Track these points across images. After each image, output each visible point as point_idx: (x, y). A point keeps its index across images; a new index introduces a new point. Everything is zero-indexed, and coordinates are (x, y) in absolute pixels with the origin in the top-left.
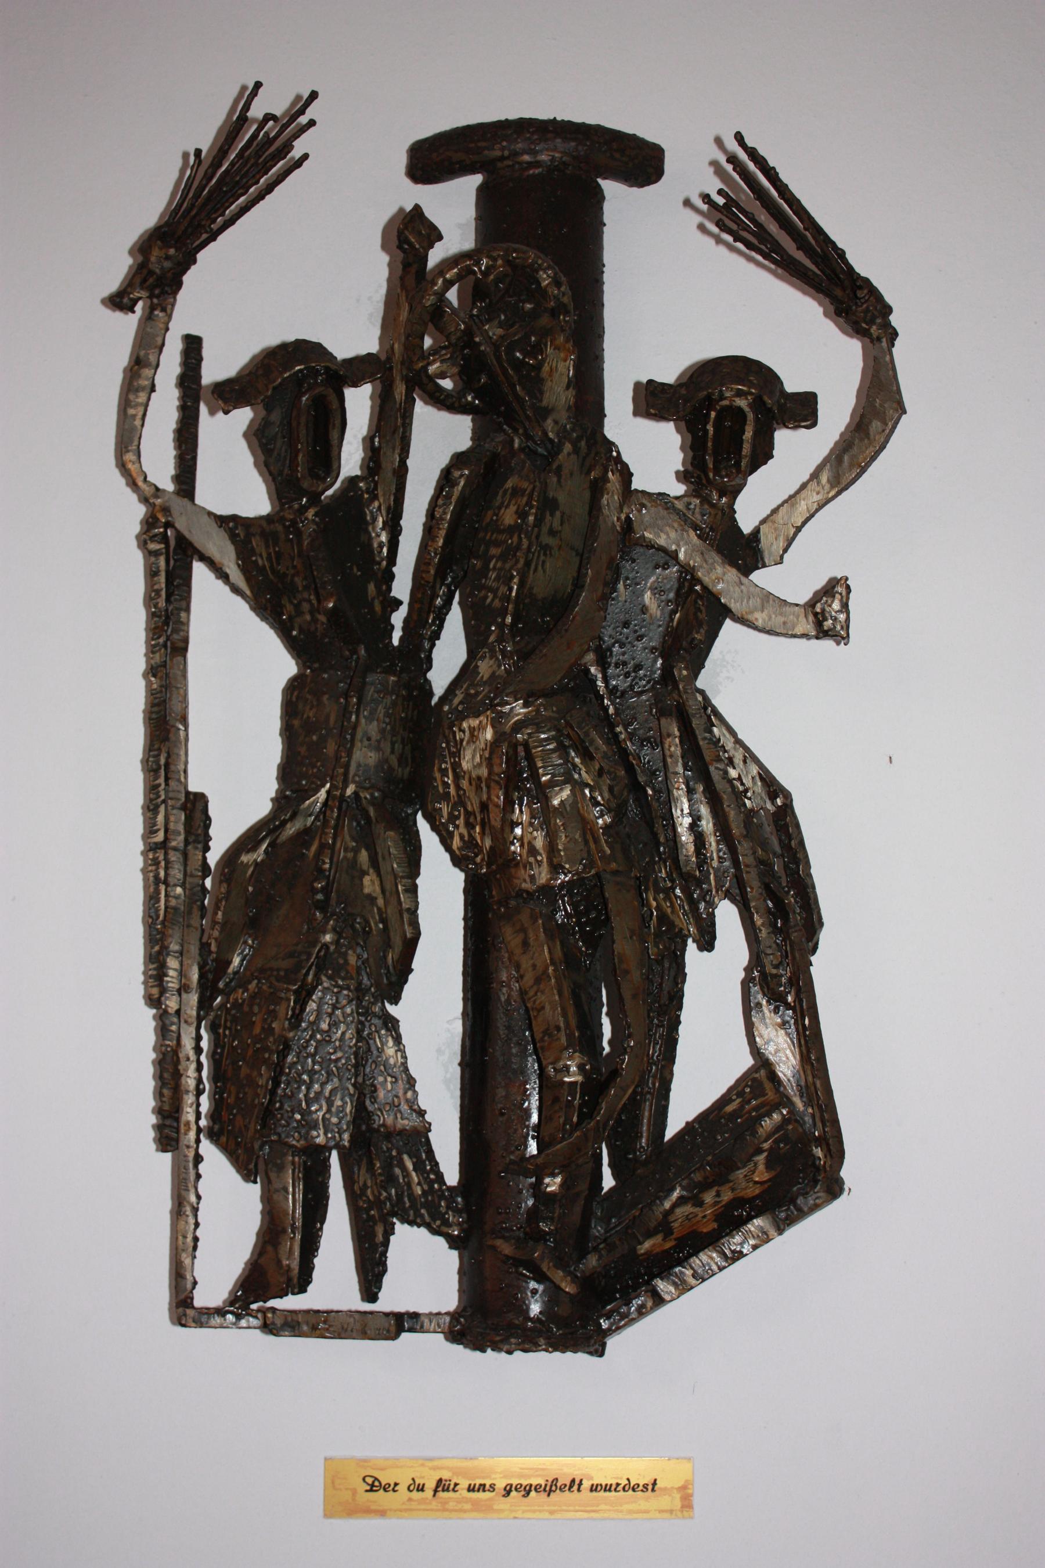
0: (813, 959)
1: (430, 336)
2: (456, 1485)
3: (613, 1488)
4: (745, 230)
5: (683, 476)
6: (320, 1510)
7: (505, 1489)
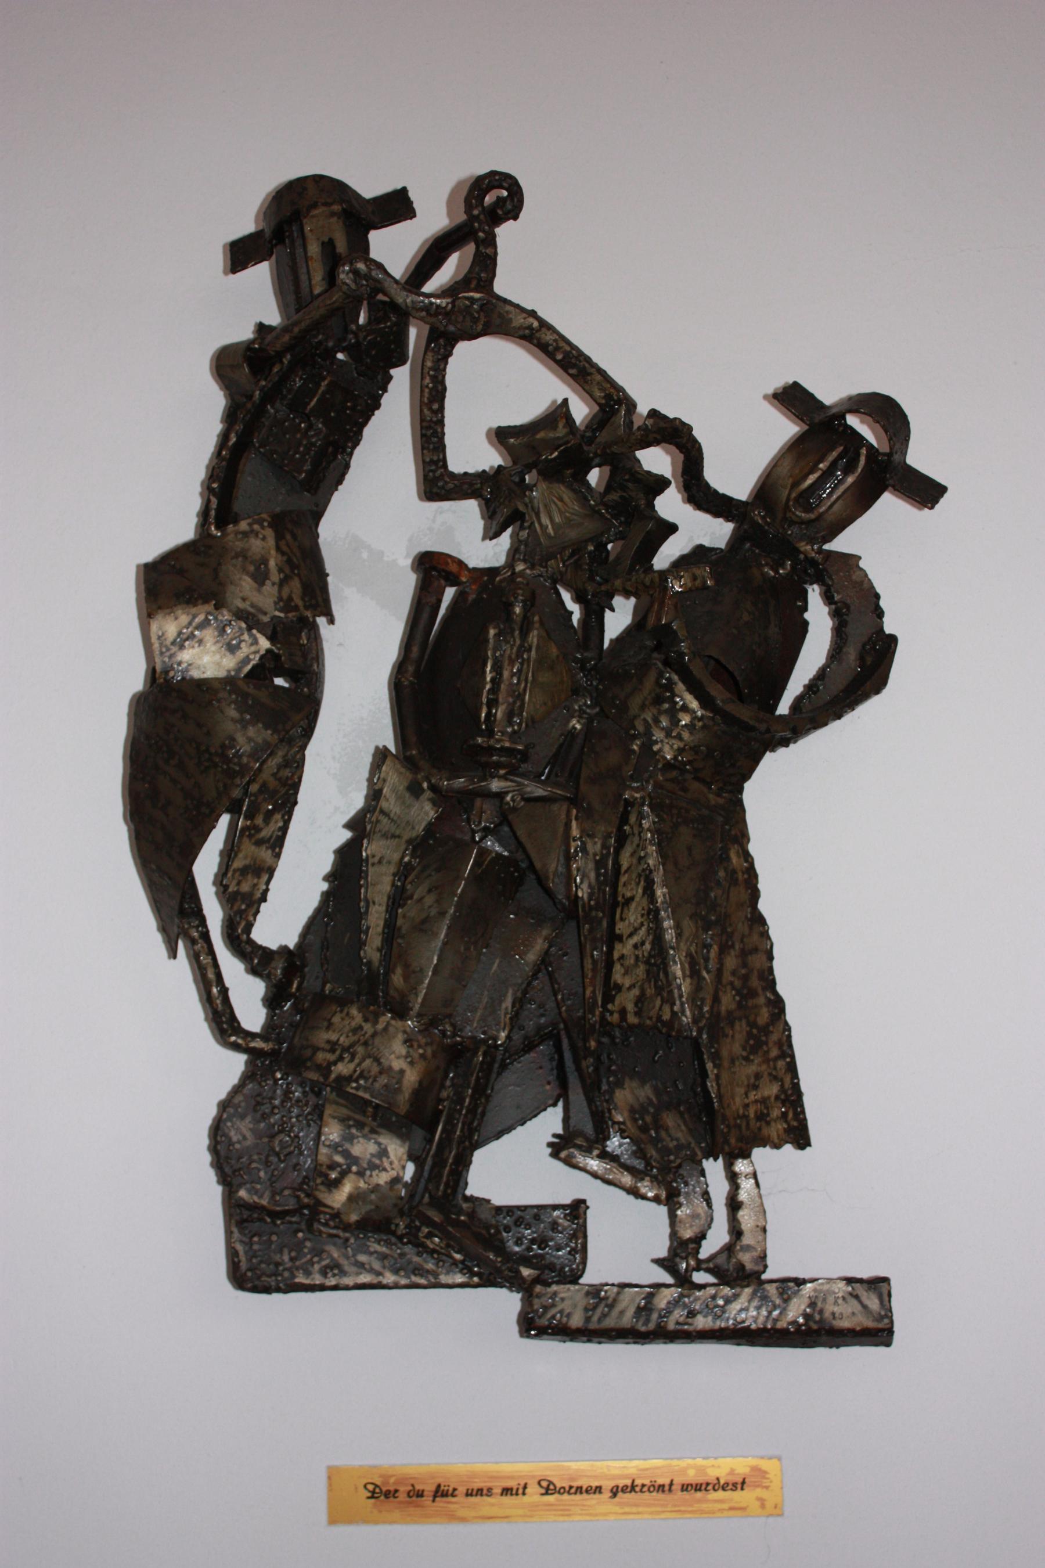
1: (416, 325)
2: (455, 1490)
5: (850, 561)
6: (323, 1517)
7: (612, 1490)
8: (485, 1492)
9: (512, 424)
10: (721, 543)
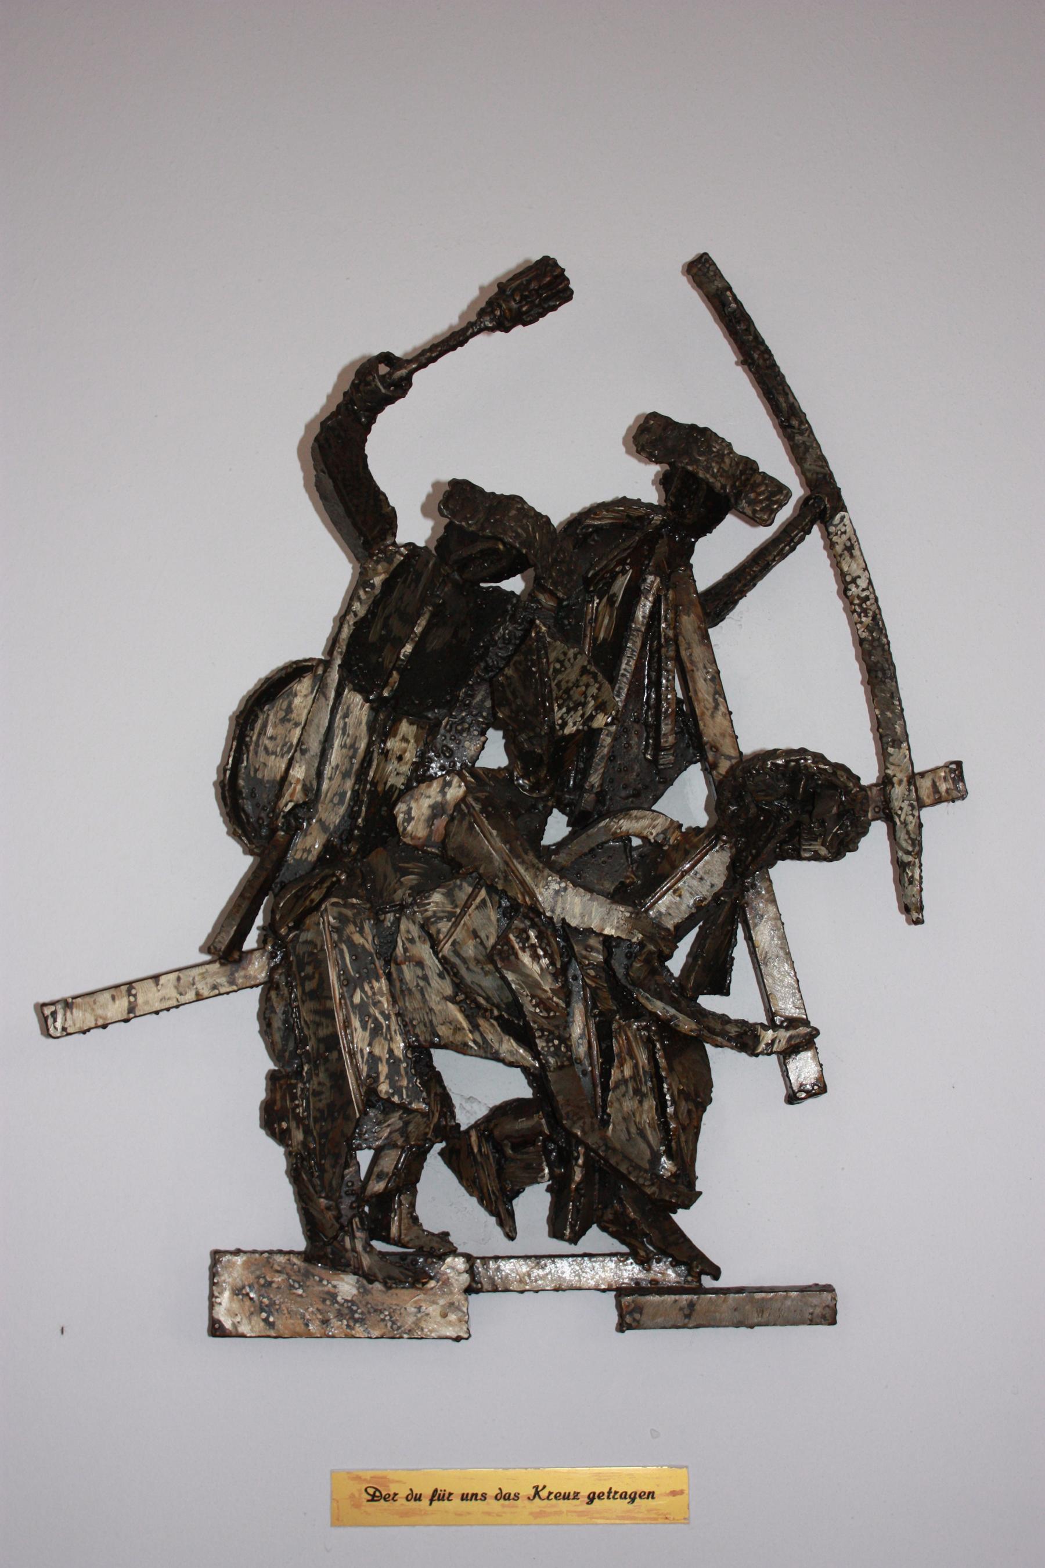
0: (271, 1066)
3: (572, 1496)
4: (593, 629)
8: (479, 1497)
9: (307, 496)
10: (565, 819)
